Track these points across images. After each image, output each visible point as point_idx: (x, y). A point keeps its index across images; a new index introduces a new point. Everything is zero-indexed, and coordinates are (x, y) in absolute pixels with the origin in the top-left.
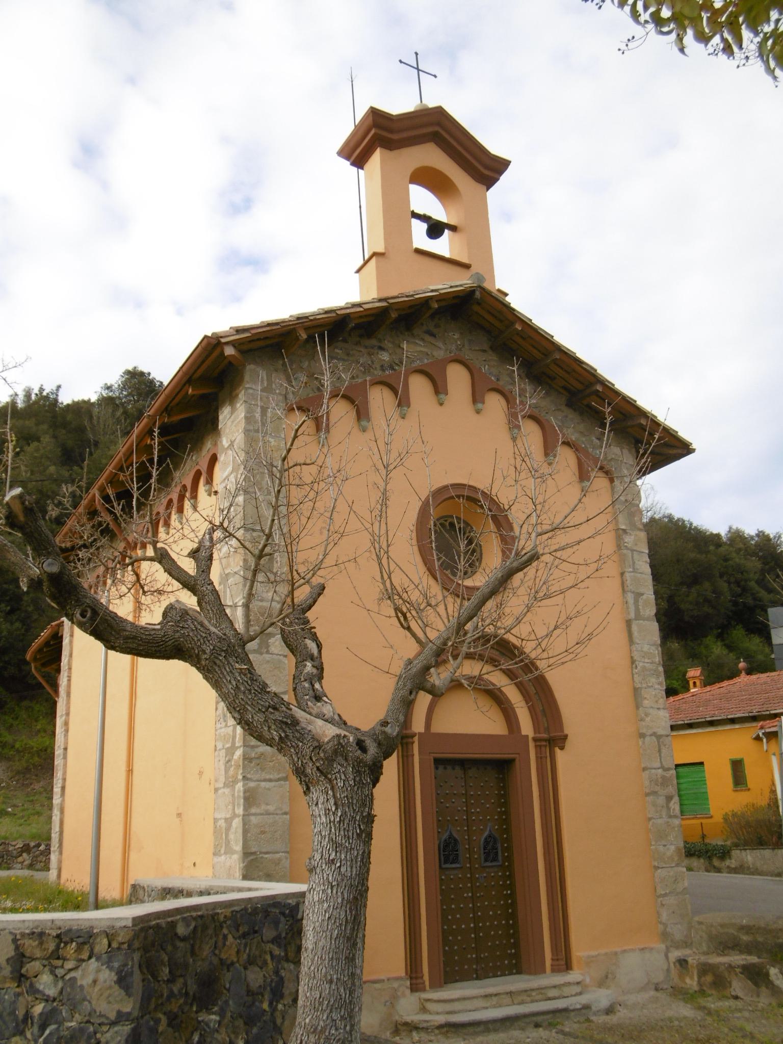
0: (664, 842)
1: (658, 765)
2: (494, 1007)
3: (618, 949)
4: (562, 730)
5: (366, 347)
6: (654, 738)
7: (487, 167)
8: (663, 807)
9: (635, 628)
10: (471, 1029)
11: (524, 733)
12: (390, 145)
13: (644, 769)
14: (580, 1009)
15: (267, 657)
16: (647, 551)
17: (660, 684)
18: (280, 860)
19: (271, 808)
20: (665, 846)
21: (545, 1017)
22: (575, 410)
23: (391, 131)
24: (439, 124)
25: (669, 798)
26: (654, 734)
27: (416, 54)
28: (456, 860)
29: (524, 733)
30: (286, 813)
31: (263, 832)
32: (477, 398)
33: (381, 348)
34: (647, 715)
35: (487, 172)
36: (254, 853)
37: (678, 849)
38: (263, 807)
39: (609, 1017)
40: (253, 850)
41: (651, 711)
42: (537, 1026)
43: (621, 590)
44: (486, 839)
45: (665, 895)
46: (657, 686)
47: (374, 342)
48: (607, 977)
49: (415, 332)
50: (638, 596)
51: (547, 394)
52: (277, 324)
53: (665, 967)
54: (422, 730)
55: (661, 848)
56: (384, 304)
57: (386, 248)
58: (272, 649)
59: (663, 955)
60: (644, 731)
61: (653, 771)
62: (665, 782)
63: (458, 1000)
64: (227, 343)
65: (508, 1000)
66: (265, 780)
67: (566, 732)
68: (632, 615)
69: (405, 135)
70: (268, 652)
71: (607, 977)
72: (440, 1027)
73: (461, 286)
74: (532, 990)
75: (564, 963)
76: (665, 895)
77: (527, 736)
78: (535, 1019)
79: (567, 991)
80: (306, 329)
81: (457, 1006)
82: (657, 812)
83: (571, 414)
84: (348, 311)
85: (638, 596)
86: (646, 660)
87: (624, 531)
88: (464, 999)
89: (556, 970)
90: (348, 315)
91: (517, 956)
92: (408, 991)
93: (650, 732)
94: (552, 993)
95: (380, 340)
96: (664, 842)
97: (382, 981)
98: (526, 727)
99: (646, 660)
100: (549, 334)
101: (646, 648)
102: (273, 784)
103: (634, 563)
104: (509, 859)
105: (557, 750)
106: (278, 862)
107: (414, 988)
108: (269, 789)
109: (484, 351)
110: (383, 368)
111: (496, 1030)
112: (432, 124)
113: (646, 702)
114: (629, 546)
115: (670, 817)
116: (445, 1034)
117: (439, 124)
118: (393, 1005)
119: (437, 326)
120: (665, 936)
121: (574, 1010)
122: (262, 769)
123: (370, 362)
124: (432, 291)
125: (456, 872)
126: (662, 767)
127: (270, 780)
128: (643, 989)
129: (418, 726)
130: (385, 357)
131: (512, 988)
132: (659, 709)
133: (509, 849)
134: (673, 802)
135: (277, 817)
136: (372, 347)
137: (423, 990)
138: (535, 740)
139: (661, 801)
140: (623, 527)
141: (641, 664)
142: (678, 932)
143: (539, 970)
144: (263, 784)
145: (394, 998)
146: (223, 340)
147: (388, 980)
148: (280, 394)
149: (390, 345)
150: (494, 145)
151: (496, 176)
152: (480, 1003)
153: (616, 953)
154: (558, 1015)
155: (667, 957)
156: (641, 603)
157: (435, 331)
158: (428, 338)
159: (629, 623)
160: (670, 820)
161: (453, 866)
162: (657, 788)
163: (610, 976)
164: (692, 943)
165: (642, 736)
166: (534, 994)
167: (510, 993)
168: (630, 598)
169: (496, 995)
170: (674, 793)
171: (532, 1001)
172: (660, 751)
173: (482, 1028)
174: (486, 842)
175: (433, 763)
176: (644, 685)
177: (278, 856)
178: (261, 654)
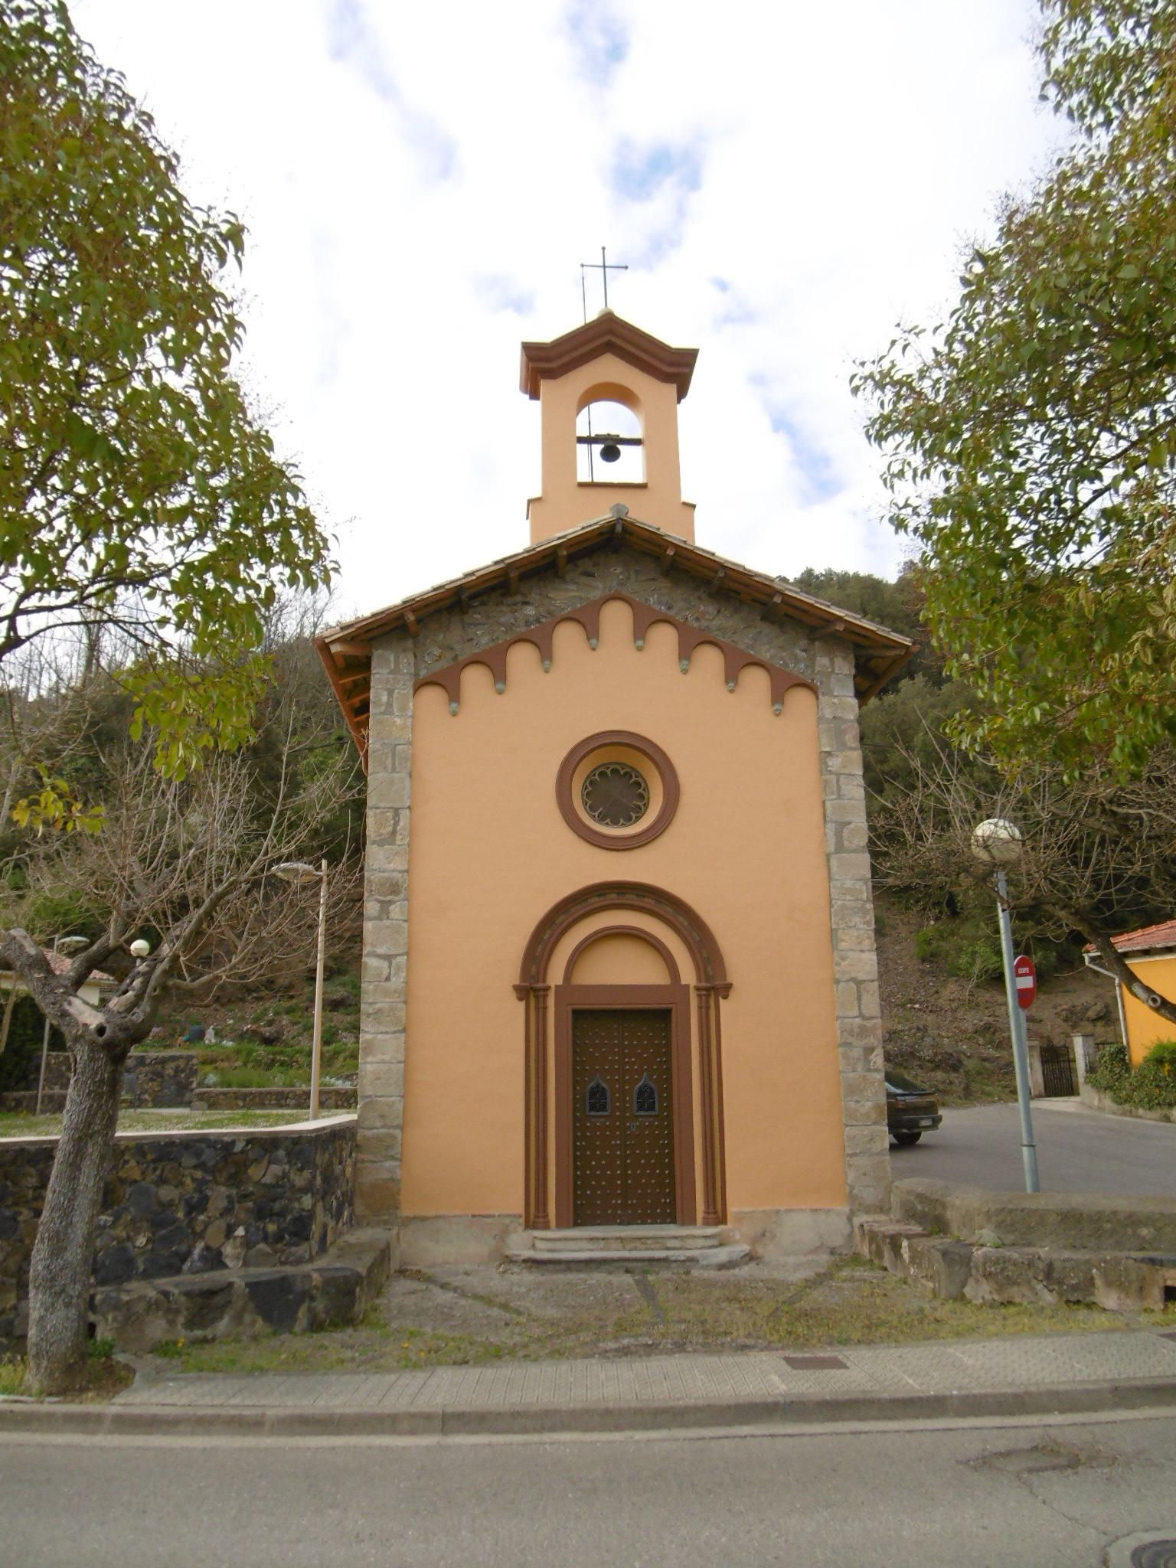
0: (856, 1098)
1: (856, 1012)
2: (602, 1249)
3: (783, 1208)
4: (724, 975)
5: (508, 605)
6: (852, 984)
7: (671, 364)
8: (858, 1059)
9: (834, 862)
10: (551, 1267)
11: (683, 982)
12: (553, 374)
13: (838, 1018)
14: (683, 1261)
15: (387, 923)
16: (861, 773)
17: (868, 923)
18: (394, 1102)
19: (387, 1057)
20: (858, 1102)
21: (639, 1264)
22: (773, 623)
23: (548, 360)
24: (611, 332)
25: (869, 1050)
26: (853, 980)
27: (604, 249)
28: (603, 1108)
29: (683, 982)
30: (400, 1062)
31: (378, 1079)
32: (640, 632)
33: (526, 603)
34: (843, 959)
35: (672, 370)
36: (370, 1096)
37: (877, 1107)
38: (380, 1057)
39: (719, 1273)
40: (369, 1093)
41: (850, 954)
42: (627, 1271)
43: (822, 820)
44: (640, 1088)
45: (855, 1155)
46: (861, 926)
47: (519, 598)
48: (763, 1235)
49: (568, 577)
50: (842, 825)
51: (736, 611)
52: (382, 613)
53: (847, 1231)
54: (560, 982)
55: (852, 1104)
56: (501, 566)
57: (544, 491)
58: (392, 915)
59: (845, 1218)
60: (838, 976)
61: (847, 1020)
62: (863, 1032)
63: (560, 1239)
64: (332, 642)
65: (618, 1245)
66: (381, 1033)
67: (730, 980)
68: (832, 848)
69: (565, 360)
70: (388, 918)
71: (763, 1235)
72: (525, 1261)
73: (564, 537)
74: (648, 1238)
75: (717, 1215)
76: (855, 1155)
77: (688, 986)
78: (627, 1264)
79: (690, 1243)
80: (414, 611)
81: (558, 1245)
82: (849, 1065)
83: (767, 629)
84: (464, 581)
85: (842, 825)
86: (848, 898)
87: (829, 753)
88: (566, 1239)
89: (707, 1223)
90: (461, 586)
91: (673, 1204)
92: (520, 1229)
93: (847, 977)
94: (671, 1243)
95: (524, 595)
96: (856, 1098)
97: (494, 1216)
98: (688, 975)
99: (848, 898)
100: (708, 552)
101: (848, 884)
102: (389, 1036)
103: (839, 788)
104: (670, 1108)
105: (722, 1001)
106: (391, 1105)
107: (529, 1225)
108: (385, 1041)
109: (654, 579)
110: (527, 623)
111: (579, 1271)
112: (600, 336)
113: (843, 945)
114: (833, 769)
115: (869, 1070)
116: (530, 1269)
117: (611, 332)
118: (503, 1239)
119: (596, 564)
120: (852, 1198)
121: (676, 1261)
122: (380, 1023)
123: (512, 621)
124: (559, 538)
125: (602, 1120)
126: (861, 1015)
127: (387, 1033)
128: (817, 1250)
129: (555, 976)
130: (530, 611)
131: (623, 1234)
132: (862, 951)
133: (669, 1099)
134: (874, 1054)
135: (392, 1066)
136: (515, 604)
137: (546, 1227)
138: (698, 989)
139: (857, 1052)
140: (827, 749)
141: (840, 903)
142: (869, 1195)
143: (692, 1222)
144: (380, 1036)
145: (505, 1233)
146: (327, 641)
147: (499, 1216)
148: (407, 673)
149: (538, 597)
150: (675, 340)
151: (686, 370)
152: (589, 1245)
153: (778, 1212)
154: (655, 1263)
155: (850, 1219)
156: (846, 832)
157: (590, 569)
158: (584, 579)
159: (828, 856)
160: (867, 1074)
161: (600, 1113)
162: (850, 1039)
163: (767, 1234)
164: (890, 1209)
165: (837, 982)
166: (649, 1242)
167: (621, 1239)
168: (830, 829)
169: (604, 1239)
170: (876, 1044)
171: (647, 1249)
172: (859, 998)
173: (563, 1266)
174: (641, 1093)
175: (570, 1017)
176: (842, 926)
177: (392, 1099)
178: (381, 920)
